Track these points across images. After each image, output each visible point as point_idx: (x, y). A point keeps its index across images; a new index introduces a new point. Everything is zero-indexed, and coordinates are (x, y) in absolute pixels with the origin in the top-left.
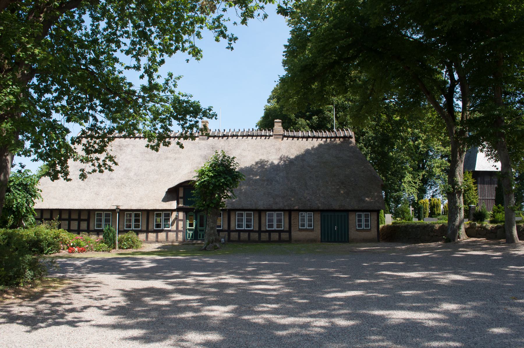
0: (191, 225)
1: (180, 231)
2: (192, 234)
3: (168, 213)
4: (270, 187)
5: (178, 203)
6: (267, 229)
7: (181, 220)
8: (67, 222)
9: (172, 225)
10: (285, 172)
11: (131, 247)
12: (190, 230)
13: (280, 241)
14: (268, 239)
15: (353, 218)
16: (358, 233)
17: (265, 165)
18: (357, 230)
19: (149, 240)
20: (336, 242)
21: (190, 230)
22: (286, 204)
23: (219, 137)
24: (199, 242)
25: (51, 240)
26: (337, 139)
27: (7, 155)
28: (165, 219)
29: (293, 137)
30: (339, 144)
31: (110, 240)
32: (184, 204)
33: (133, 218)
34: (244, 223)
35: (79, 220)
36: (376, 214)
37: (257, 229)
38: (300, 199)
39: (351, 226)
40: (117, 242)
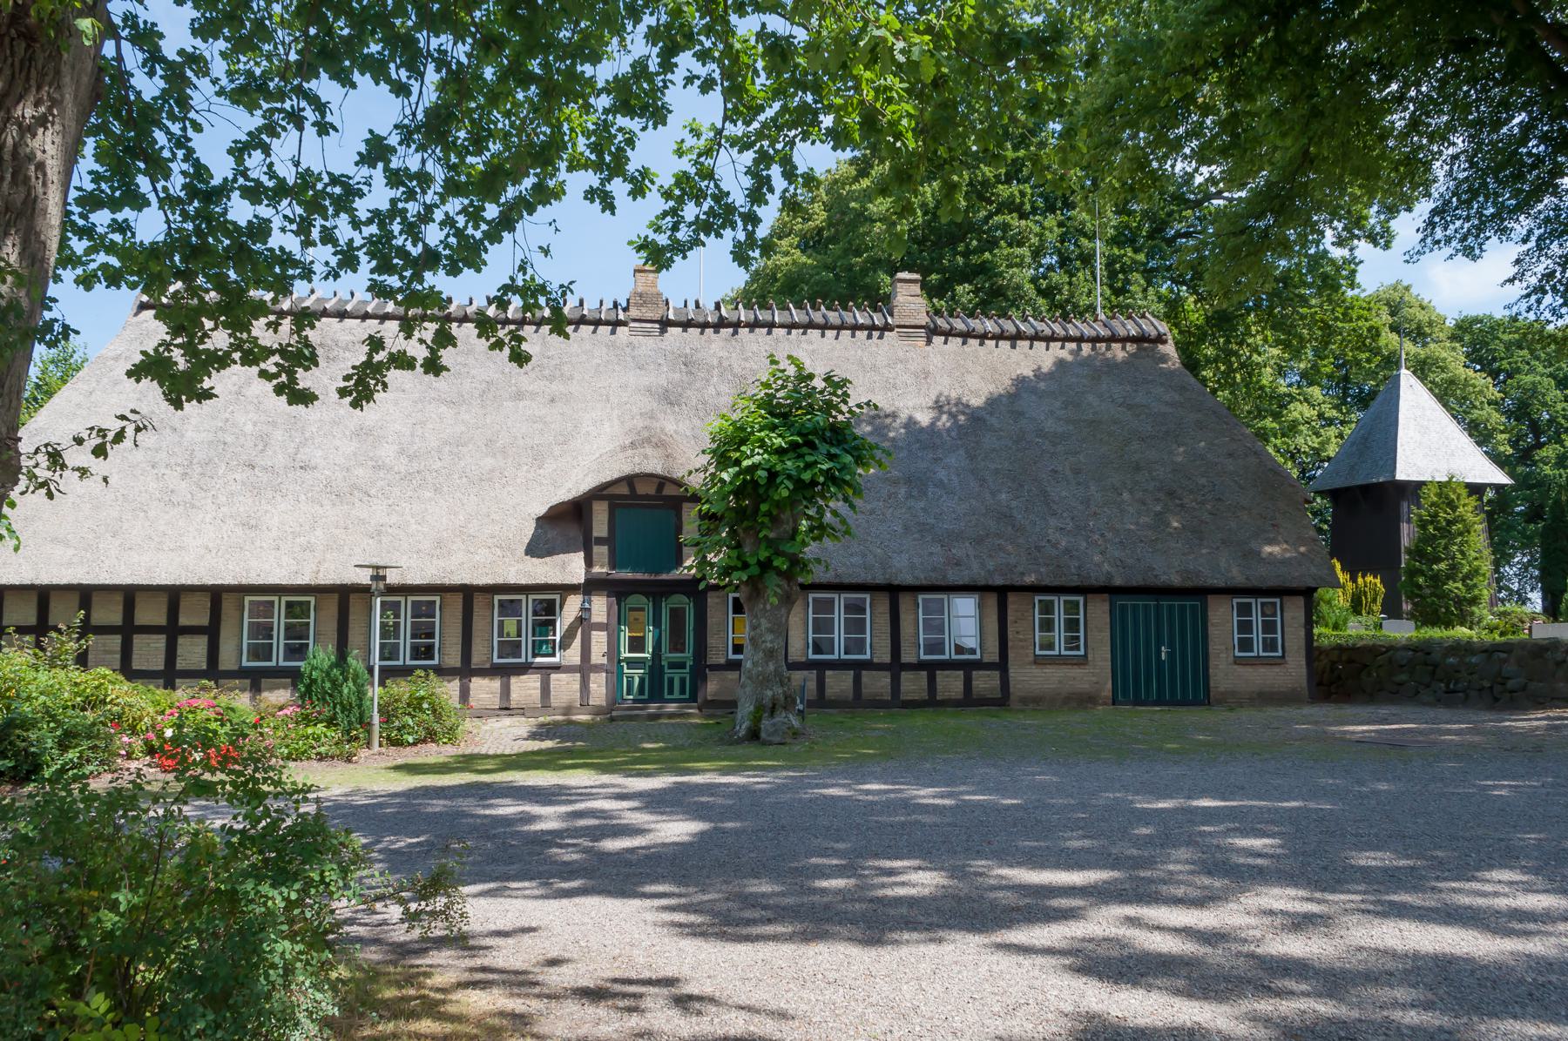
0: (637, 644)
1: (597, 668)
2: (642, 680)
3: (547, 599)
4: (922, 504)
5: (589, 562)
6: (923, 657)
7: (600, 627)
8: (116, 641)
9: (565, 644)
10: (962, 452)
11: (431, 736)
12: (632, 663)
13: (969, 700)
14: (925, 695)
15: (1222, 618)
16: (1240, 669)
17: (888, 427)
18: (1238, 661)
19: (472, 703)
20: (1159, 702)
21: (632, 663)
22: (991, 565)
23: (704, 326)
24: (672, 708)
25: (72, 719)
26: (1116, 346)
27: (42, 122)
28: (536, 624)
29: (966, 336)
30: (1125, 362)
31: (346, 709)
32: (613, 567)
33: (279, 621)
34: (839, 636)
35: (173, 631)
36: (1300, 601)
37: (887, 659)
38: (1038, 549)
39: (1214, 648)
40: (376, 719)
